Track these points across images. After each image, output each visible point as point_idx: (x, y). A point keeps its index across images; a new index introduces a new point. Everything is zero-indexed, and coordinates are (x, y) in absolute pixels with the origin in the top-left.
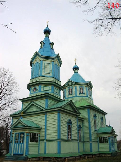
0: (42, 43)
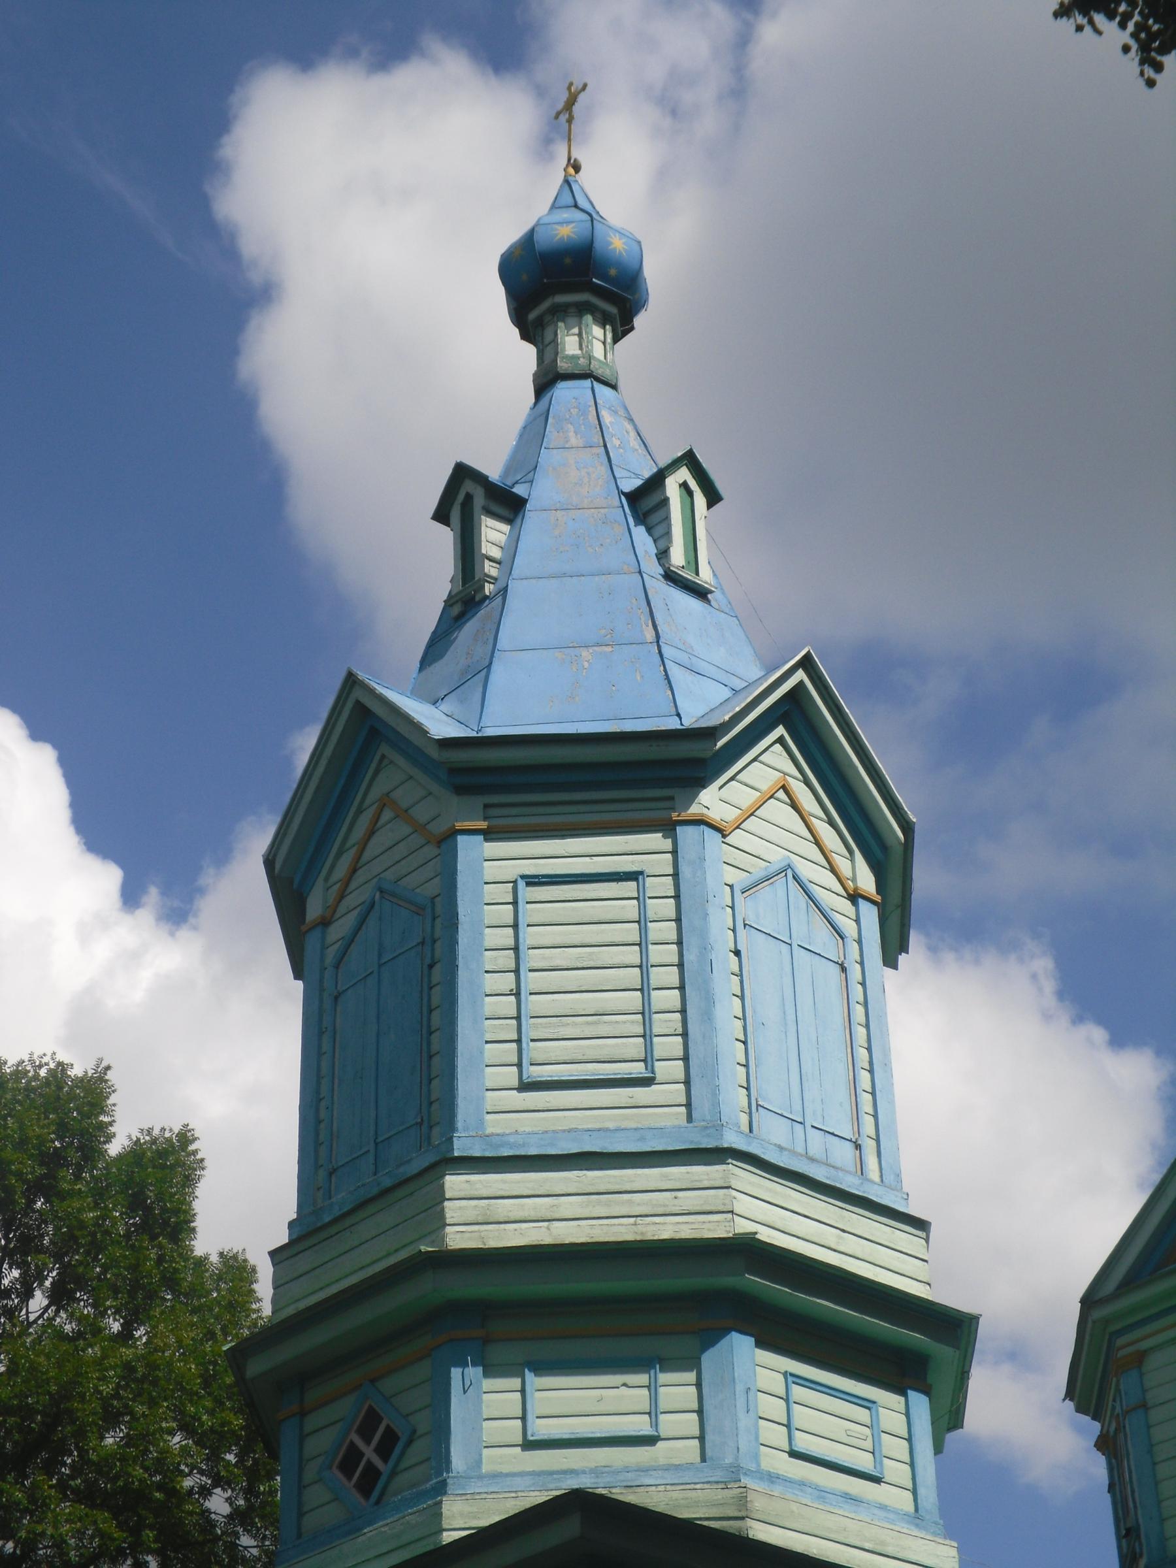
0: (479, 499)
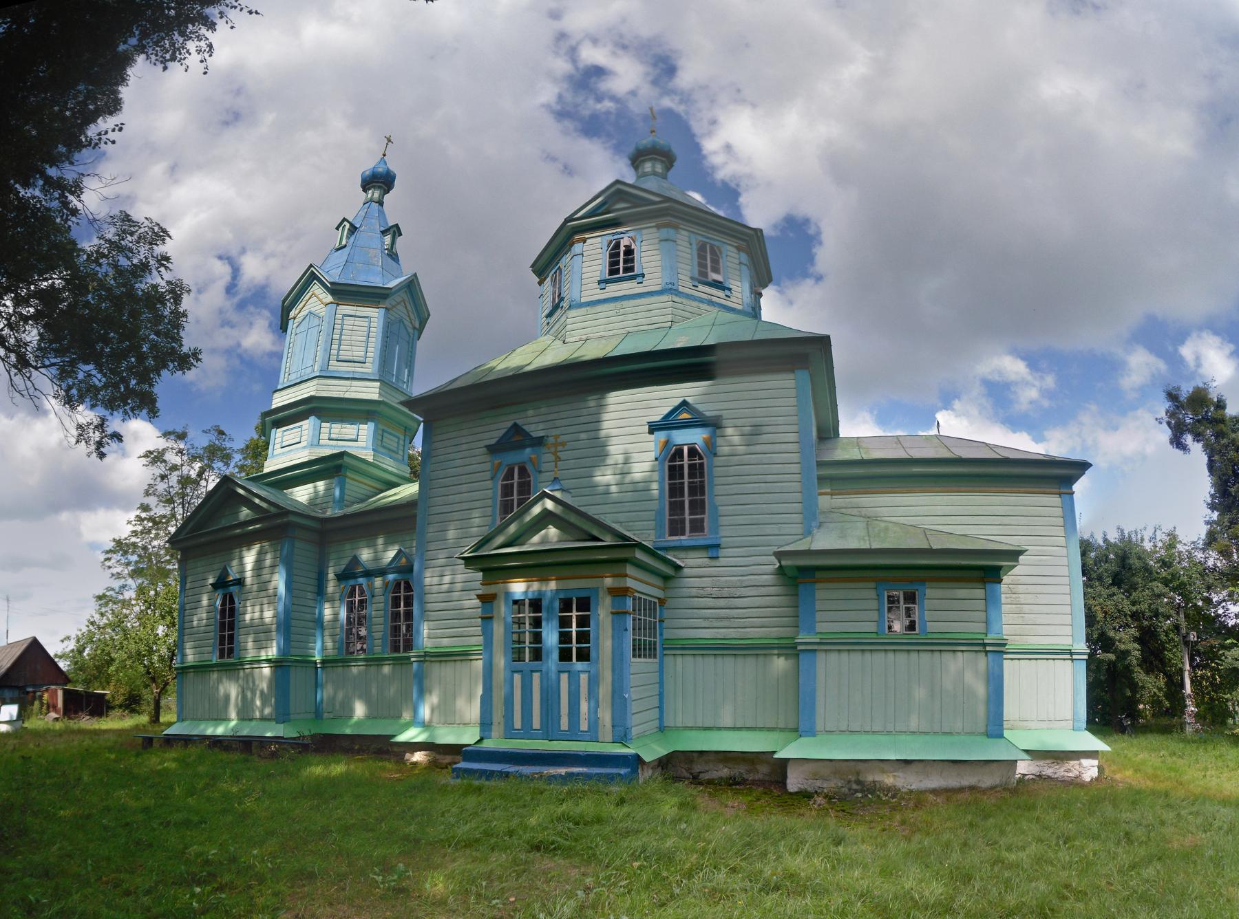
0: (348, 226)
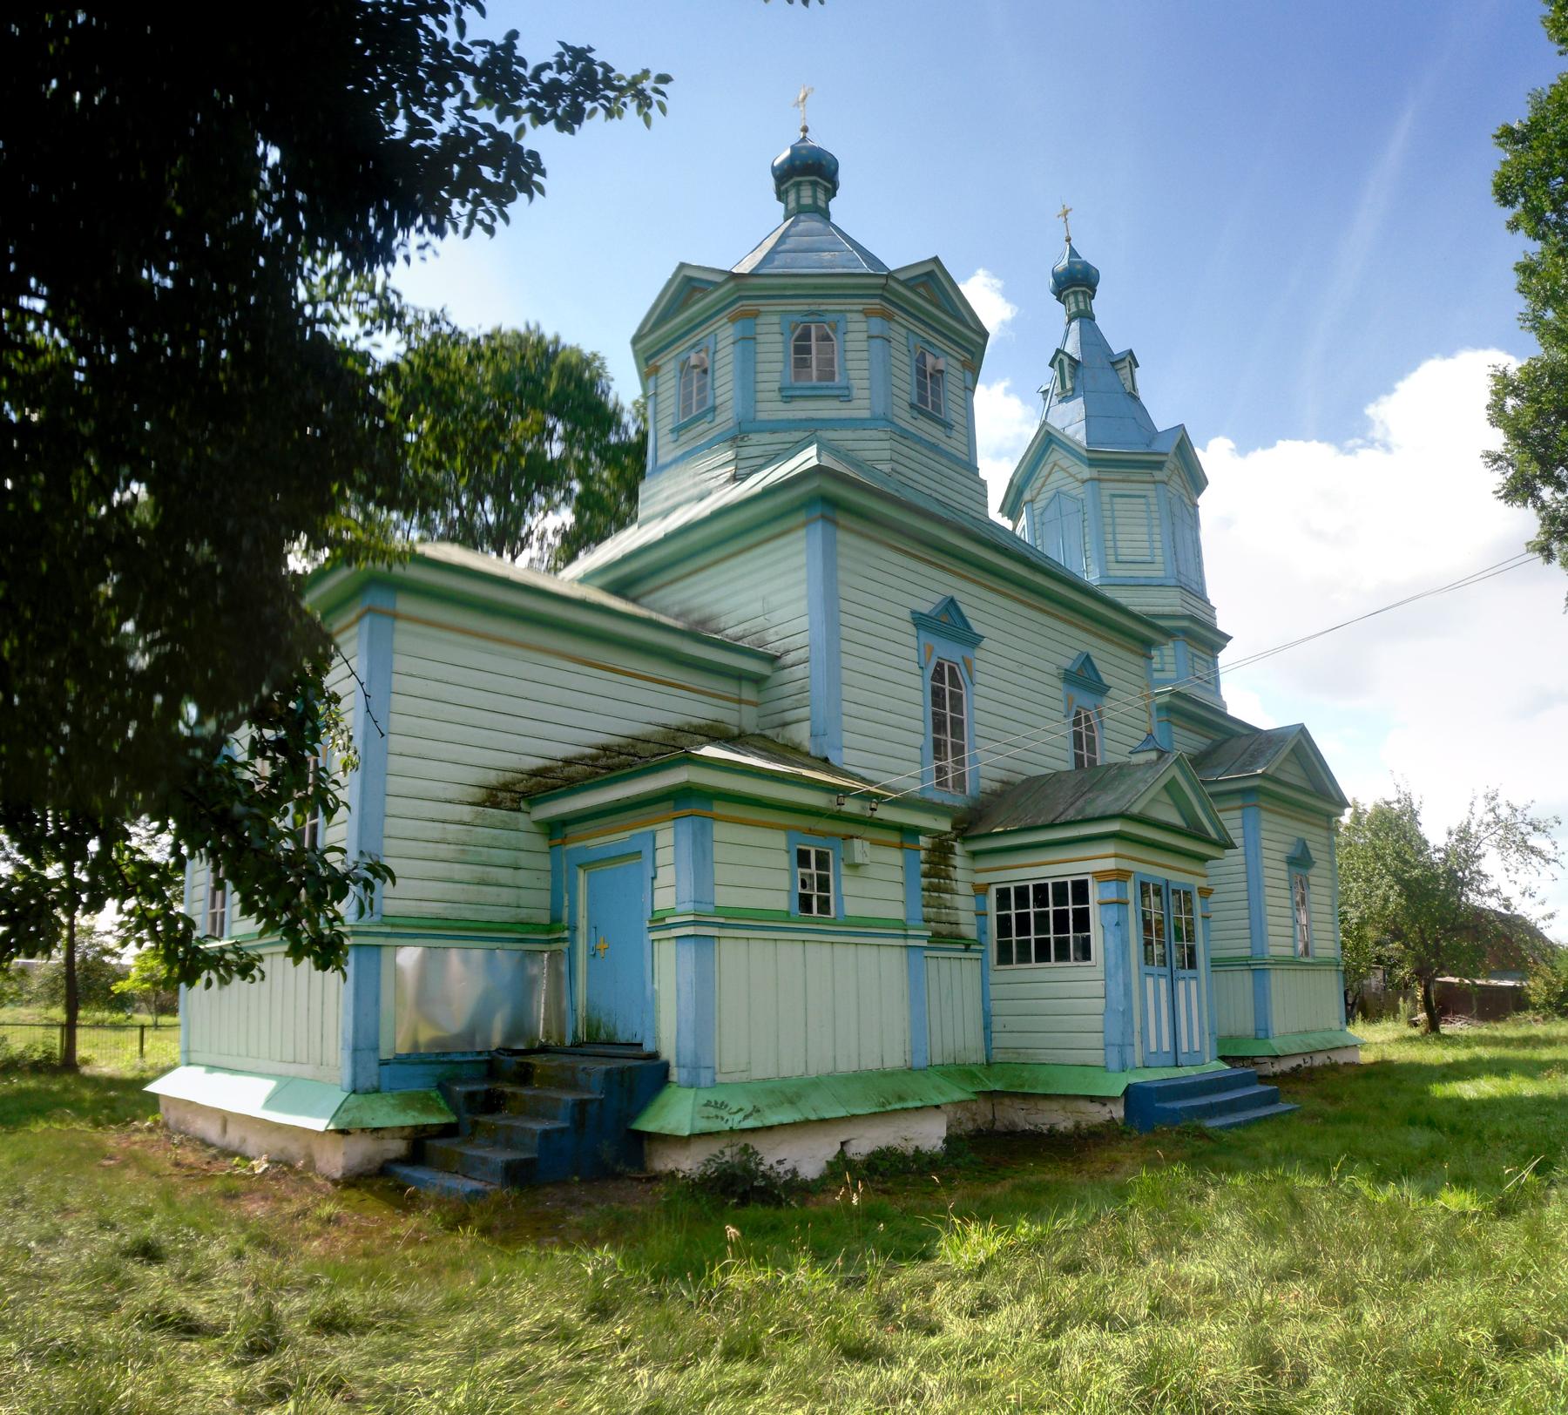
0: (1066, 361)
